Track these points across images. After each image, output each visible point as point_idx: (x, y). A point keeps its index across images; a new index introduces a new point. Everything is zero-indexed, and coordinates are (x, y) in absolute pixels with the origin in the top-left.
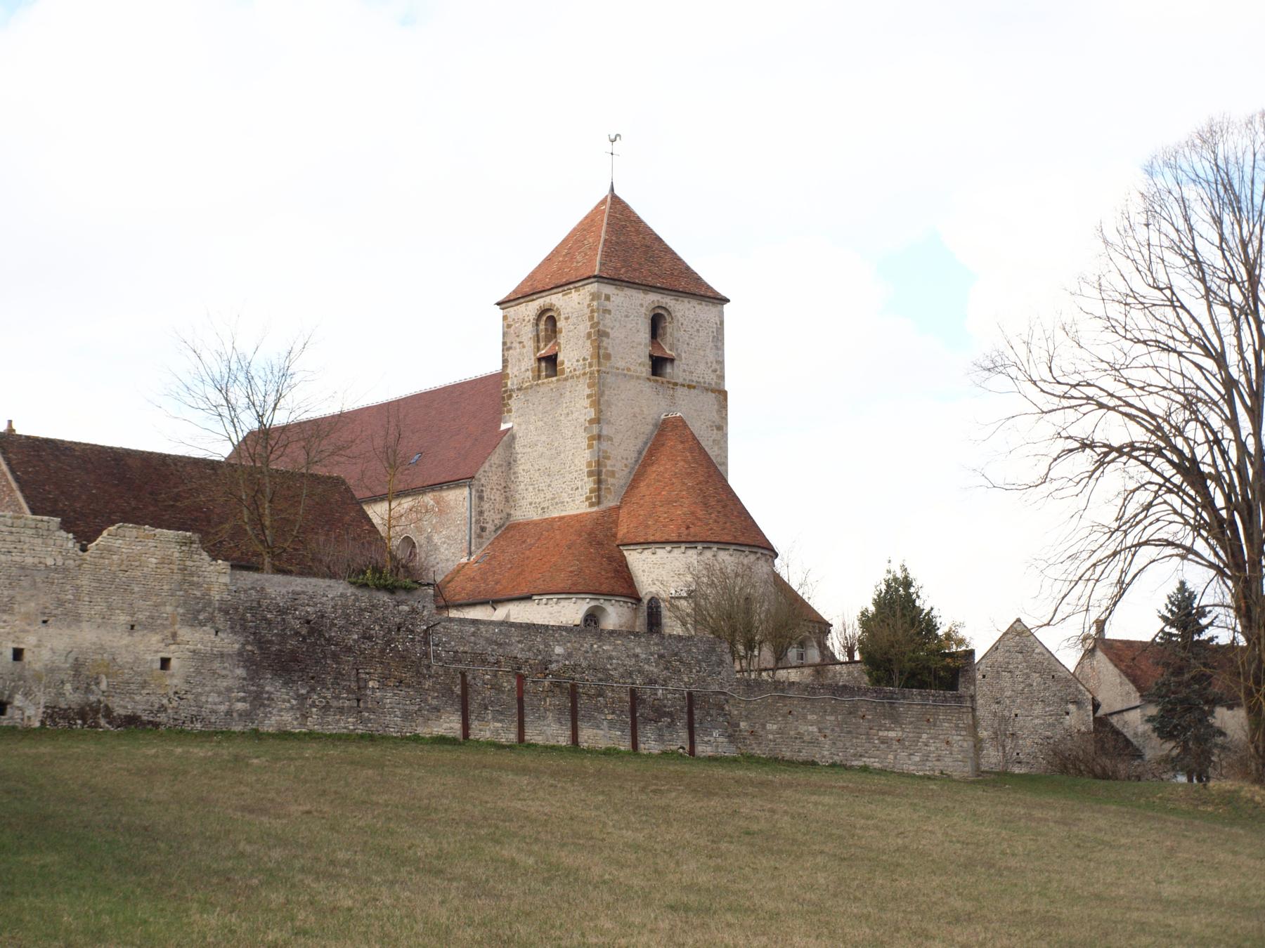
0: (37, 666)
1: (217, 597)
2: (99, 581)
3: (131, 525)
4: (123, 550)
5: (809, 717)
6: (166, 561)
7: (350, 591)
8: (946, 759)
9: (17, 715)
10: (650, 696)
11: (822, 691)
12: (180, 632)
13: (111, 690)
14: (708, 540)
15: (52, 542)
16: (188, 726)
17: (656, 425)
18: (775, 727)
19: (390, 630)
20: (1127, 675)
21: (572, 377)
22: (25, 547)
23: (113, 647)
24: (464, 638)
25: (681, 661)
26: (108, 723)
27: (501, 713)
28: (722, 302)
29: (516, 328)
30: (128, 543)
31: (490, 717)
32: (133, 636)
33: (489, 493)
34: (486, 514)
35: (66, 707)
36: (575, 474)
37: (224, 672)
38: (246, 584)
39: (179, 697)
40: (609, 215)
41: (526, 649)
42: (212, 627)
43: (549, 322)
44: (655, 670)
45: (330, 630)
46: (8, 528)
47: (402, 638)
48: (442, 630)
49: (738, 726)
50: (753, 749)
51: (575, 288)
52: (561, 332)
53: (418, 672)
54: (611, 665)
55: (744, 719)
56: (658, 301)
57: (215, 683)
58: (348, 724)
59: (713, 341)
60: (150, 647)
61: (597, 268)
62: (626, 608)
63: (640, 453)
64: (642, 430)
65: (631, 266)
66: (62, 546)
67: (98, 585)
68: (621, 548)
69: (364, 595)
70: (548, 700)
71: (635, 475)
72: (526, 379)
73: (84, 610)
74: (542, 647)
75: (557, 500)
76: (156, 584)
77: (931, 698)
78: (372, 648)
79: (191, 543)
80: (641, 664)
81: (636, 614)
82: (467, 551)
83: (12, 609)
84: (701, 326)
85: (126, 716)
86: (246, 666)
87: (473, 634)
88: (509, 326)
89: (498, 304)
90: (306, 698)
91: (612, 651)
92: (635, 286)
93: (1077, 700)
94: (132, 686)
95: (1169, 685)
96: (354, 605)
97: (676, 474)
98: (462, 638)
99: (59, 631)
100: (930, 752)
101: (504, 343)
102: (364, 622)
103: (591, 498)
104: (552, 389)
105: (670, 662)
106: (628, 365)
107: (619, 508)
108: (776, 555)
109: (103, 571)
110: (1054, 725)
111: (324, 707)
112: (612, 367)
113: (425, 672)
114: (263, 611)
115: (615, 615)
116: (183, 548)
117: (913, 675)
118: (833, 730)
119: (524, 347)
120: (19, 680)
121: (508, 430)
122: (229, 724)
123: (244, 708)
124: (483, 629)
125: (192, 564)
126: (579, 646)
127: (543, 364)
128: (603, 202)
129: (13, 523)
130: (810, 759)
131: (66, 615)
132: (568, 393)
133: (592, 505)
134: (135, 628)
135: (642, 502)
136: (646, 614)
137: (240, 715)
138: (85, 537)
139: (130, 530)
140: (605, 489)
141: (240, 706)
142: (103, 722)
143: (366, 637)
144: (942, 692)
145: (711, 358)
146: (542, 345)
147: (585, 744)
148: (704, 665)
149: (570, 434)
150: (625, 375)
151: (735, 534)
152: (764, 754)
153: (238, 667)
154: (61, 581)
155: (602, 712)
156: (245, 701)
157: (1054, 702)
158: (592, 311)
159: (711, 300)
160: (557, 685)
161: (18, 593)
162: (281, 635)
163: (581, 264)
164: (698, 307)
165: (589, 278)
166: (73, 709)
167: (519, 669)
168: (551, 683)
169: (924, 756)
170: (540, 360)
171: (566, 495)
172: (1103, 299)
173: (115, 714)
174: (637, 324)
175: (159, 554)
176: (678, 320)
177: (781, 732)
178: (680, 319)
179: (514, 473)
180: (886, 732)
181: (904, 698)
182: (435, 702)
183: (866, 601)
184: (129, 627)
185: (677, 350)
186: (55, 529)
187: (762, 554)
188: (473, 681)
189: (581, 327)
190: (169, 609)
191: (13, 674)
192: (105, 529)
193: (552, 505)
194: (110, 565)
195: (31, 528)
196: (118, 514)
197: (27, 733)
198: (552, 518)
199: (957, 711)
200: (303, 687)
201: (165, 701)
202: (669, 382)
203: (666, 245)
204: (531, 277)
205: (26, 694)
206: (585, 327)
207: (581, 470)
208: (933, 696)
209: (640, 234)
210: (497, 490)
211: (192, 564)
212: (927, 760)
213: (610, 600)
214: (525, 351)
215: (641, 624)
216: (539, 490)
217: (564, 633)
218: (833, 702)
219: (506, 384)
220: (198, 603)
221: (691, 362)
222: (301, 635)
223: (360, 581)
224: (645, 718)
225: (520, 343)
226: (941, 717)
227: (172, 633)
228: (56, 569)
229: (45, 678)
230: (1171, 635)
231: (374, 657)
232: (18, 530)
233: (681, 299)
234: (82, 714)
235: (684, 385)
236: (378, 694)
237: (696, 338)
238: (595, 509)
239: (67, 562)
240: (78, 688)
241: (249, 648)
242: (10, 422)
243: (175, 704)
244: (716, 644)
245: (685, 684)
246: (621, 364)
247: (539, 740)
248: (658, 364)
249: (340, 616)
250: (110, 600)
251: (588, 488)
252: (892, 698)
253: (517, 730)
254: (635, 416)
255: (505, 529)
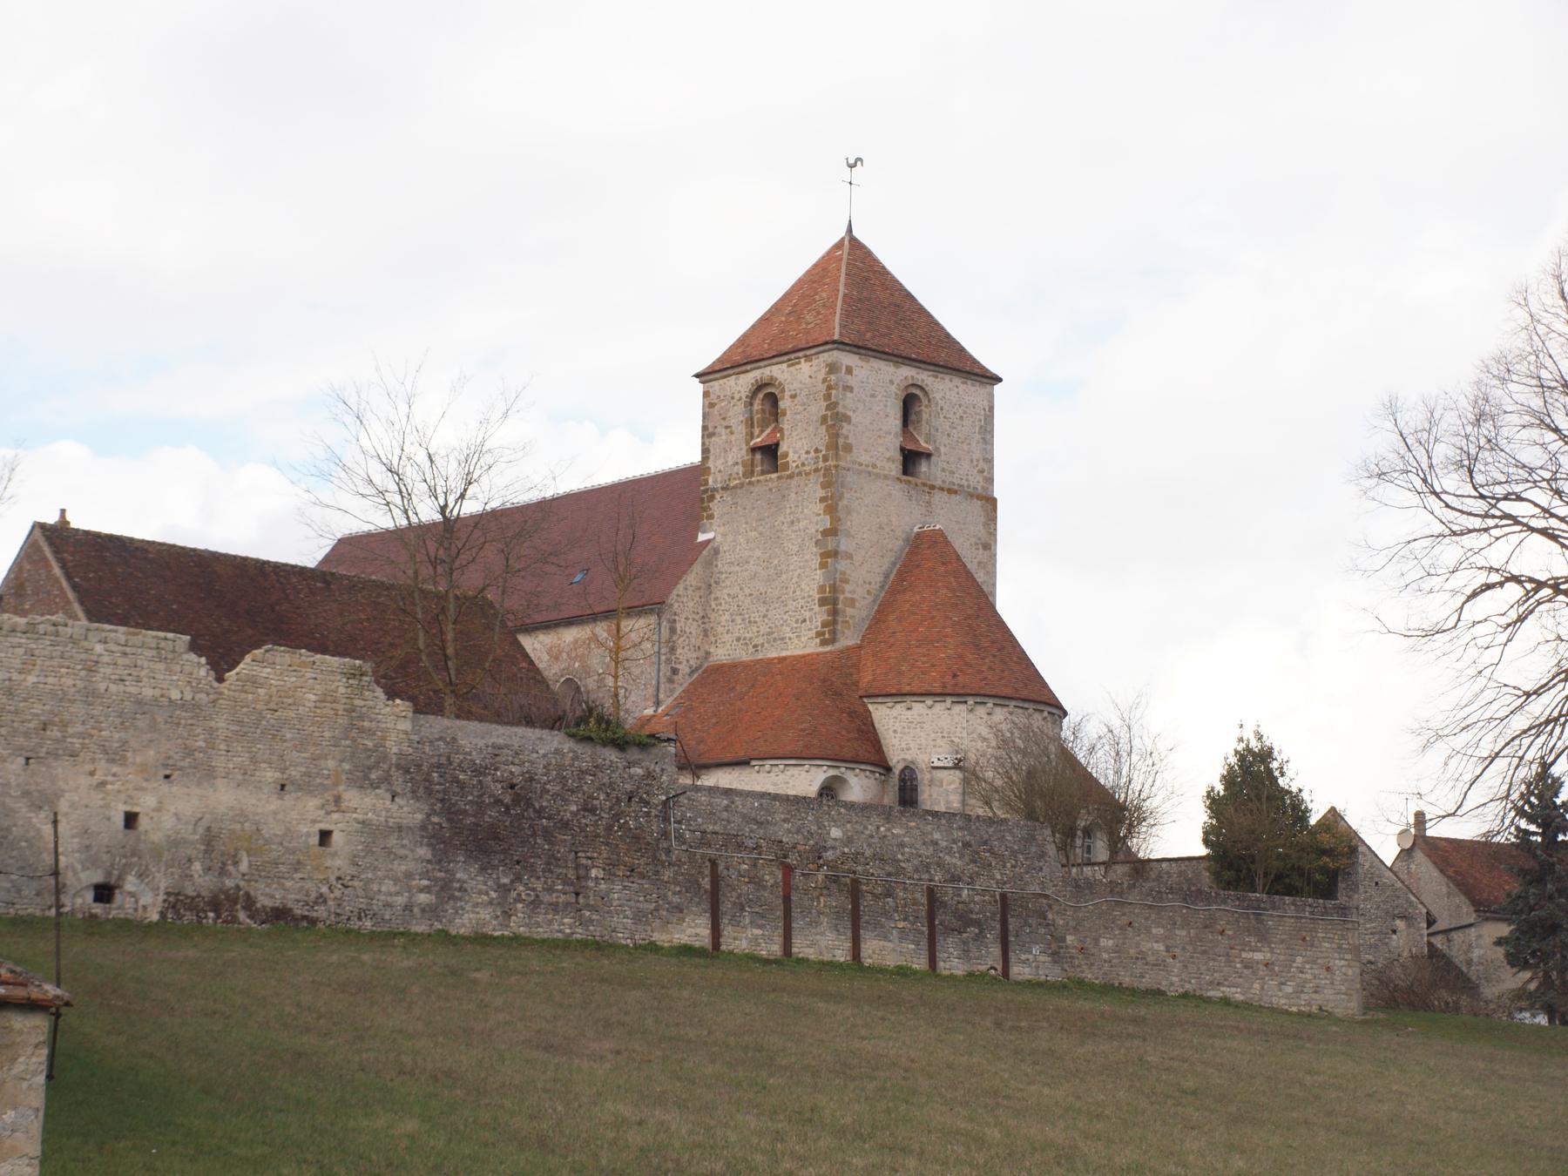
0: (156, 837)
1: (395, 750)
2: (240, 723)
3: (282, 648)
4: (272, 682)
5: (1154, 931)
6: (329, 698)
7: (568, 745)
8: (1326, 991)
9: (129, 903)
10: (952, 898)
11: (1170, 896)
12: (346, 796)
13: (254, 872)
14: (982, 692)
15: (178, 668)
16: (355, 924)
17: (907, 540)
18: (1111, 943)
19: (618, 800)
20: (1458, 885)
21: (800, 474)
22: (143, 673)
23: (258, 814)
24: (714, 814)
25: (991, 851)
26: (249, 917)
27: (763, 917)
28: (994, 382)
29: (722, 408)
30: (278, 672)
31: (747, 921)
32: (283, 800)
33: (683, 624)
34: (679, 651)
35: (195, 894)
36: (802, 602)
37: (402, 852)
38: (432, 733)
39: (342, 885)
40: (848, 264)
41: (793, 830)
42: (387, 790)
43: (769, 399)
44: (959, 863)
45: (541, 797)
46: (120, 648)
47: (634, 811)
48: (686, 801)
49: (1063, 939)
50: (1082, 972)
51: (806, 356)
52: (785, 414)
53: (655, 857)
54: (902, 854)
55: (1072, 931)
56: (913, 377)
57: (390, 866)
58: (563, 926)
59: (979, 433)
60: (306, 815)
61: (837, 331)
62: (872, 780)
63: (887, 576)
64: (890, 546)
65: (878, 331)
66: (191, 674)
67: (237, 728)
68: (865, 700)
69: (585, 750)
70: (822, 899)
71: (880, 605)
72: (734, 476)
73: (220, 763)
74: (814, 828)
75: (775, 635)
76: (316, 729)
77: (1307, 909)
78: (596, 824)
79: (361, 675)
80: (941, 855)
81: (883, 788)
82: (654, 700)
83: (124, 758)
84: (965, 412)
85: (273, 909)
86: (432, 844)
87: (726, 809)
88: (712, 405)
89: (697, 376)
90: (510, 890)
91: (904, 836)
92: (885, 356)
93: (1407, 914)
94: (282, 868)
95: (1527, 898)
96: (573, 765)
97: (937, 604)
98: (711, 813)
99: (187, 790)
100: (1306, 981)
101: (705, 428)
102: (585, 788)
103: (823, 634)
104: (770, 490)
105: (977, 853)
106: (874, 460)
107: (860, 647)
108: (1065, 714)
109: (245, 710)
110: (1376, 946)
111: (532, 902)
112: (854, 462)
113: (664, 858)
114: (455, 769)
115: (859, 787)
116: (351, 681)
117: (1279, 877)
118: (1184, 948)
119: (732, 433)
120: (133, 855)
121: (708, 541)
122: (408, 923)
123: (428, 901)
124: (739, 803)
125: (362, 703)
126: (862, 828)
127: (758, 456)
128: (839, 246)
129: (127, 641)
130: (1155, 987)
131: (195, 768)
132: (793, 496)
133: (824, 643)
134: (286, 788)
135: (892, 640)
136: (897, 788)
137: (423, 911)
138: (221, 662)
139: (282, 656)
140: (843, 622)
141: (423, 898)
142: (242, 916)
143: (588, 809)
144: (1321, 901)
145: (977, 455)
146: (756, 431)
147: (869, 960)
148: (1021, 857)
149: (795, 548)
150: (869, 473)
151: (1016, 686)
152: (1097, 979)
153: (421, 845)
154: (190, 722)
155: (890, 918)
156: (428, 892)
157: (1377, 917)
158: (829, 388)
159: (979, 379)
160: (834, 880)
161: (133, 736)
162: (477, 803)
163: (812, 325)
164: (962, 387)
165: (826, 343)
166: (203, 898)
167: (785, 857)
168: (826, 876)
169: (1298, 985)
170: (754, 450)
171: (788, 629)
172: (850, 183)
173: (258, 905)
174: (886, 406)
175: (319, 689)
176: (937, 404)
177: (1117, 950)
178: (940, 402)
179: (716, 599)
180: (1251, 953)
181: (1274, 908)
182: (676, 899)
183: (1212, 776)
184: (279, 787)
185: (935, 442)
186: (182, 650)
187: (1049, 713)
188: (725, 872)
189: (813, 409)
190: (331, 763)
191: (123, 847)
192: (248, 652)
193: (768, 642)
194: (255, 701)
195: (151, 648)
196: (207, 638)
197: (146, 929)
198: (768, 659)
199: (1340, 927)
200: (506, 875)
201: (324, 889)
202: (924, 484)
203: (920, 305)
204: (743, 341)
205: (141, 875)
206: (818, 408)
207: (809, 596)
208: (1310, 906)
209: (887, 289)
210: (694, 620)
211: (362, 703)
212: (1302, 992)
213: (854, 769)
214: (733, 438)
215: (891, 798)
216: (750, 622)
217: (842, 810)
218: (1184, 911)
219: (707, 481)
220: (370, 757)
221: (952, 459)
222: (502, 804)
223: (581, 733)
224: (946, 928)
225: (727, 427)
226: (1320, 935)
227: (335, 796)
228: (183, 706)
229: (166, 853)
230: (1526, 832)
231: (597, 836)
232: (134, 650)
233: (942, 375)
234: (215, 905)
235: (942, 489)
236: (603, 886)
237: (959, 428)
238: (827, 648)
239: (198, 696)
240: (209, 869)
241: (435, 819)
242: (63, 512)
243: (337, 893)
244: (1035, 830)
245: (997, 883)
246: (865, 458)
247: (811, 953)
248: (911, 459)
249: (554, 780)
250: (254, 749)
251: (820, 620)
252: (1258, 908)
253: (781, 939)
254: (881, 527)
255: (703, 673)
